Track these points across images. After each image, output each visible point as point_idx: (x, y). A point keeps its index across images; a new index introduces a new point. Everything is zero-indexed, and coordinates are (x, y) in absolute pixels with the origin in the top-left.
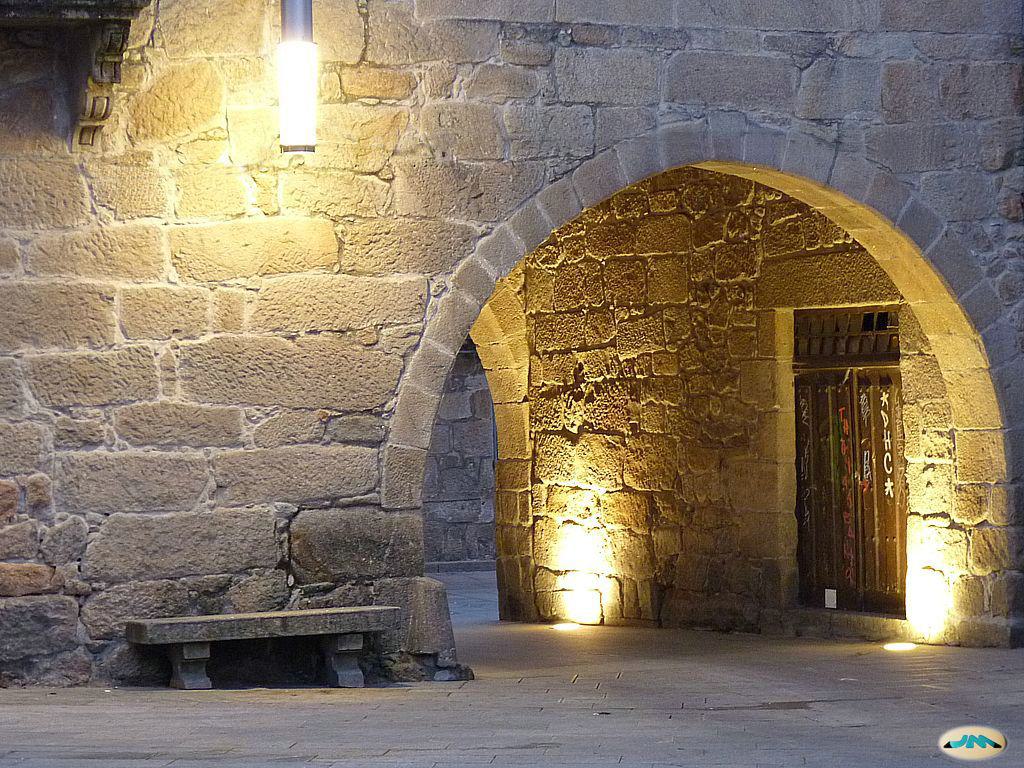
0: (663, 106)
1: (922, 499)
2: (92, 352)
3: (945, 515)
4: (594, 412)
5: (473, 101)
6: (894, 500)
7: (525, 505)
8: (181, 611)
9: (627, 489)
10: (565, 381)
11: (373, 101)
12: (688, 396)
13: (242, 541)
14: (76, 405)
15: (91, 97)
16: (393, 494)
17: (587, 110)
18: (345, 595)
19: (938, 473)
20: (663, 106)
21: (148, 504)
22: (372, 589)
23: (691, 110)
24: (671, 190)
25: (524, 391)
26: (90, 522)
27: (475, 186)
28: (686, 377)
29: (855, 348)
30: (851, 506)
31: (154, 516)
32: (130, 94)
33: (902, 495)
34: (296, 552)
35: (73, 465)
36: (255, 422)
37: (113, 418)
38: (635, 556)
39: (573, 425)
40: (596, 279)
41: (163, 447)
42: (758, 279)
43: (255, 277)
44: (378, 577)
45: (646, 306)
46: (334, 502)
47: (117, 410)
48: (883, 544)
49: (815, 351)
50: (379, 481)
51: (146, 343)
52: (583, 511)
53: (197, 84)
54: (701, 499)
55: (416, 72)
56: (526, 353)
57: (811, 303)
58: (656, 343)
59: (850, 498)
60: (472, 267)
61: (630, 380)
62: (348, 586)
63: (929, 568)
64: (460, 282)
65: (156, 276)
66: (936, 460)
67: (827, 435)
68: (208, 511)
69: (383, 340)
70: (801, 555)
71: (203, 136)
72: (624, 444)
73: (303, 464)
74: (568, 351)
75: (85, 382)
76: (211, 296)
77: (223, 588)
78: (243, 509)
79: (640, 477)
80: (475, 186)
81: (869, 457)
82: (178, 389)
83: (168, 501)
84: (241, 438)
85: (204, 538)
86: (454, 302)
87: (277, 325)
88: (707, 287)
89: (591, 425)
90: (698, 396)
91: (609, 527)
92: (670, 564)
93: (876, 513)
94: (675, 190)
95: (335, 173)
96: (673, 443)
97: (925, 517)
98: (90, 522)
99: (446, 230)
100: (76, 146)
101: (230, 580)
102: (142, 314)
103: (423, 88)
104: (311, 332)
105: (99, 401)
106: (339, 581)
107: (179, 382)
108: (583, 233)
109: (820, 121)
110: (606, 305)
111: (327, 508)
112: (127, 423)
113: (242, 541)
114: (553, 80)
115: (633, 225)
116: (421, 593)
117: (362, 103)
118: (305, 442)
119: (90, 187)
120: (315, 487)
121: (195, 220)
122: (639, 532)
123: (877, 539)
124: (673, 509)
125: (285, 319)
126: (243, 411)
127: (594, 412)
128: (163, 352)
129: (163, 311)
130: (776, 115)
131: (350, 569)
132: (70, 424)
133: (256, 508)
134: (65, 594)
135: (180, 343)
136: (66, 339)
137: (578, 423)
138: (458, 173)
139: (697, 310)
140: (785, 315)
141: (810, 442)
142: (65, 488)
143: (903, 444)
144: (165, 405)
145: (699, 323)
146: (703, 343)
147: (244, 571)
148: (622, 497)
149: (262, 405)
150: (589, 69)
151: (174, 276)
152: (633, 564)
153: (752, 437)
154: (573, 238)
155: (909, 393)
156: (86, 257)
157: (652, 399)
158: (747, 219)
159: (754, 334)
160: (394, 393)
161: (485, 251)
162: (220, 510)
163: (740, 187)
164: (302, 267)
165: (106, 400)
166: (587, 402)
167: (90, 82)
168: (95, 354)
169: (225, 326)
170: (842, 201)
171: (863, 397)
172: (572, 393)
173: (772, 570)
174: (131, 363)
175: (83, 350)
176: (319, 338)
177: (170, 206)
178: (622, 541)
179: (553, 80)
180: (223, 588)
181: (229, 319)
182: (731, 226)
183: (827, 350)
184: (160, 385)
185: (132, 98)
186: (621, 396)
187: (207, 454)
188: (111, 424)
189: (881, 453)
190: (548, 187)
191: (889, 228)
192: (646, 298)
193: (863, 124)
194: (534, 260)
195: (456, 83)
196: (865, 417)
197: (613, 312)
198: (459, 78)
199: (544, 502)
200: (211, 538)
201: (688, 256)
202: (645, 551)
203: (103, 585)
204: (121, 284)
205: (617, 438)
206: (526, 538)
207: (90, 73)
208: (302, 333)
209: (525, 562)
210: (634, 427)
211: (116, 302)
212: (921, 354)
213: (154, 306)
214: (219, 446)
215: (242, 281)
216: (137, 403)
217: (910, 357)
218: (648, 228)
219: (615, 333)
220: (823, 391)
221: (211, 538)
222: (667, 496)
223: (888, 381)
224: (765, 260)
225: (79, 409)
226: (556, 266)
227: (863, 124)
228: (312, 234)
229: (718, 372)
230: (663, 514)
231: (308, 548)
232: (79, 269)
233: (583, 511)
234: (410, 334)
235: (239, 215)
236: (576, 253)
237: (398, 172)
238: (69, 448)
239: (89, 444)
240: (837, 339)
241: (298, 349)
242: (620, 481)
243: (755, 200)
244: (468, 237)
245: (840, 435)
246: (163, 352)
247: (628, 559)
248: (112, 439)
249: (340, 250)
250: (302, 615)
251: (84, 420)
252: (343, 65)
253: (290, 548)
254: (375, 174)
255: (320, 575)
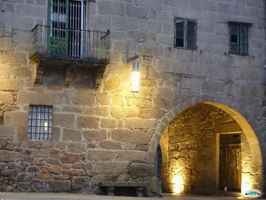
0: (201, 90)
1: (244, 170)
2: (95, 130)
3: (249, 172)
4: (181, 154)
5: (166, 87)
6: (239, 170)
7: (167, 171)
8: (109, 181)
9: (186, 168)
10: (175, 148)
11: (148, 86)
12: (199, 150)
13: (121, 168)
14: (92, 140)
15: (98, 81)
16: (149, 160)
17: (187, 90)
18: (139, 180)
19: (248, 164)
20: (201, 90)
21: (104, 160)
22: (144, 179)
23: (206, 91)
24: (196, 112)
25: (167, 150)
26: (93, 162)
27: (166, 103)
28: (198, 147)
29: (231, 141)
30: (230, 171)
31: (105, 162)
32: (104, 82)
33: (240, 169)
34: (131, 171)
35: (90, 151)
36: (124, 145)
37: (98, 143)
38: (188, 181)
39: (177, 156)
40: (182, 129)
41: (107, 149)
42: (213, 128)
43: (126, 117)
44: (146, 176)
45: (191, 134)
46: (138, 161)
47: (99, 141)
48: (237, 179)
49: (224, 142)
50: (147, 158)
51: (105, 129)
52: (178, 172)
53: (116, 80)
54: (201, 170)
55: (156, 81)
56: (168, 143)
57: (223, 133)
58: (193, 140)
59: (230, 170)
60: (165, 118)
61: (188, 148)
62: (140, 178)
63: (246, 183)
64: (163, 121)
65: (107, 116)
66: (248, 162)
67: (226, 158)
68: (115, 162)
69: (148, 131)
70: (220, 181)
71: (117, 90)
72: (186, 160)
73: (132, 154)
74: (176, 142)
75: (93, 136)
76: (117, 121)
77: (117, 177)
78: (121, 162)
79: (189, 166)
80: (166, 103)
81: (234, 162)
82: (110, 138)
83: (108, 159)
84: (122, 148)
85: (114, 167)
86: (161, 125)
87: (129, 127)
88: (203, 130)
89: (180, 156)
90: (201, 151)
91: (183, 175)
92: (194, 182)
93: (235, 172)
94: (198, 112)
95: (141, 99)
96: (196, 159)
97: (245, 173)
98: (93, 162)
99: (161, 111)
100: (94, 91)
101: (118, 175)
102: (104, 123)
103: (157, 84)
104: (135, 129)
105: (96, 139)
106: (138, 177)
107: (111, 137)
108: (180, 121)
109: (229, 95)
110: (184, 134)
111: (137, 162)
112: (101, 144)
113: (121, 168)
114: (181, 84)
115: (189, 119)
116: (154, 180)
117: (146, 86)
118: (133, 150)
119: (96, 99)
120: (135, 158)
121: (115, 106)
122: (189, 176)
123: (235, 178)
124: (195, 172)
125: (131, 126)
126: (122, 143)
127: (181, 154)
128: (108, 131)
129: (108, 123)
130: (221, 93)
131: (141, 175)
132: (90, 143)
133: (124, 162)
134: (88, 176)
135: (111, 129)
136: (90, 127)
137: (178, 156)
138: (163, 100)
139: (201, 134)
140: (218, 135)
141: (222, 159)
142: (89, 156)
143: (241, 159)
144: (108, 141)
145: (201, 137)
146: (202, 140)
147: (121, 174)
148: (185, 170)
149: (126, 142)
150: (188, 83)
151: (111, 116)
152: (187, 182)
153: (211, 158)
154: (178, 122)
155: (242, 149)
156: (95, 112)
157: (192, 151)
158: (211, 117)
159: (212, 138)
160: (150, 141)
161: (168, 115)
162: (117, 162)
163: (212, 108)
164: (134, 116)
165: (97, 139)
166: (179, 152)
167: (97, 78)
168: (95, 130)
169: (120, 126)
170: (232, 110)
171: (233, 150)
172: (177, 150)
173: (215, 183)
174: (102, 132)
175: (93, 129)
176: (137, 130)
177: (111, 103)
178: (185, 178)
179: (181, 84)
180: (117, 177)
181: (120, 125)
182: (208, 119)
183: (226, 142)
184: (107, 137)
185: (105, 82)
186: (186, 151)
187: (115, 151)
188: (98, 144)
189: (236, 161)
190: (179, 104)
191: (241, 116)
192: (191, 132)
193: (237, 96)
194: (170, 126)
195: (163, 83)
196: (233, 154)
197: (185, 135)
198: (164, 82)
199: (171, 171)
200: (115, 167)
201: (199, 124)
202: (190, 180)
203: (95, 175)
204: (101, 117)
205: (185, 159)
206: (167, 177)
207: (97, 76)
208: (134, 129)
209: (167, 182)
210: (188, 156)
211: (100, 121)
212: (245, 142)
213: (107, 122)
214: (117, 149)
215: (123, 118)
216: (103, 140)
217: (243, 142)
218: (192, 119)
219: (185, 139)
220: (225, 150)
221: (115, 167)
222: (194, 169)
223: (239, 147)
224: (215, 125)
225: (92, 141)
226: (174, 127)
227: (237, 96)
228: (136, 110)
229: (205, 146)
230: (193, 173)
231: (133, 170)
232: (94, 114)
233: (178, 172)
234: (153, 130)
235: (123, 106)
236: (178, 124)
237: (152, 99)
238: (90, 148)
239: (94, 147)
240: (228, 140)
241: (133, 132)
242: (185, 166)
243: (213, 114)
244: (164, 112)
245: (228, 157)
246: (108, 131)
247: (186, 181)
248: (98, 147)
249: (141, 113)
250: (132, 182)
251: (93, 143)
252: (143, 79)
253: (130, 170)
254: (148, 99)
255: (135, 175)
